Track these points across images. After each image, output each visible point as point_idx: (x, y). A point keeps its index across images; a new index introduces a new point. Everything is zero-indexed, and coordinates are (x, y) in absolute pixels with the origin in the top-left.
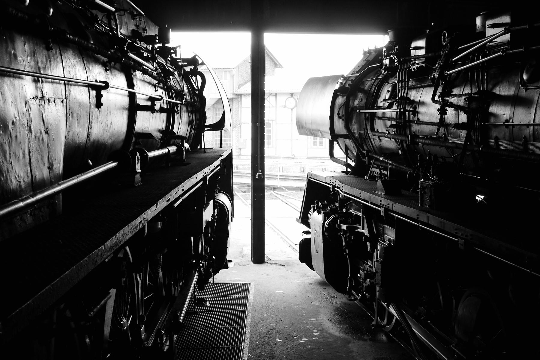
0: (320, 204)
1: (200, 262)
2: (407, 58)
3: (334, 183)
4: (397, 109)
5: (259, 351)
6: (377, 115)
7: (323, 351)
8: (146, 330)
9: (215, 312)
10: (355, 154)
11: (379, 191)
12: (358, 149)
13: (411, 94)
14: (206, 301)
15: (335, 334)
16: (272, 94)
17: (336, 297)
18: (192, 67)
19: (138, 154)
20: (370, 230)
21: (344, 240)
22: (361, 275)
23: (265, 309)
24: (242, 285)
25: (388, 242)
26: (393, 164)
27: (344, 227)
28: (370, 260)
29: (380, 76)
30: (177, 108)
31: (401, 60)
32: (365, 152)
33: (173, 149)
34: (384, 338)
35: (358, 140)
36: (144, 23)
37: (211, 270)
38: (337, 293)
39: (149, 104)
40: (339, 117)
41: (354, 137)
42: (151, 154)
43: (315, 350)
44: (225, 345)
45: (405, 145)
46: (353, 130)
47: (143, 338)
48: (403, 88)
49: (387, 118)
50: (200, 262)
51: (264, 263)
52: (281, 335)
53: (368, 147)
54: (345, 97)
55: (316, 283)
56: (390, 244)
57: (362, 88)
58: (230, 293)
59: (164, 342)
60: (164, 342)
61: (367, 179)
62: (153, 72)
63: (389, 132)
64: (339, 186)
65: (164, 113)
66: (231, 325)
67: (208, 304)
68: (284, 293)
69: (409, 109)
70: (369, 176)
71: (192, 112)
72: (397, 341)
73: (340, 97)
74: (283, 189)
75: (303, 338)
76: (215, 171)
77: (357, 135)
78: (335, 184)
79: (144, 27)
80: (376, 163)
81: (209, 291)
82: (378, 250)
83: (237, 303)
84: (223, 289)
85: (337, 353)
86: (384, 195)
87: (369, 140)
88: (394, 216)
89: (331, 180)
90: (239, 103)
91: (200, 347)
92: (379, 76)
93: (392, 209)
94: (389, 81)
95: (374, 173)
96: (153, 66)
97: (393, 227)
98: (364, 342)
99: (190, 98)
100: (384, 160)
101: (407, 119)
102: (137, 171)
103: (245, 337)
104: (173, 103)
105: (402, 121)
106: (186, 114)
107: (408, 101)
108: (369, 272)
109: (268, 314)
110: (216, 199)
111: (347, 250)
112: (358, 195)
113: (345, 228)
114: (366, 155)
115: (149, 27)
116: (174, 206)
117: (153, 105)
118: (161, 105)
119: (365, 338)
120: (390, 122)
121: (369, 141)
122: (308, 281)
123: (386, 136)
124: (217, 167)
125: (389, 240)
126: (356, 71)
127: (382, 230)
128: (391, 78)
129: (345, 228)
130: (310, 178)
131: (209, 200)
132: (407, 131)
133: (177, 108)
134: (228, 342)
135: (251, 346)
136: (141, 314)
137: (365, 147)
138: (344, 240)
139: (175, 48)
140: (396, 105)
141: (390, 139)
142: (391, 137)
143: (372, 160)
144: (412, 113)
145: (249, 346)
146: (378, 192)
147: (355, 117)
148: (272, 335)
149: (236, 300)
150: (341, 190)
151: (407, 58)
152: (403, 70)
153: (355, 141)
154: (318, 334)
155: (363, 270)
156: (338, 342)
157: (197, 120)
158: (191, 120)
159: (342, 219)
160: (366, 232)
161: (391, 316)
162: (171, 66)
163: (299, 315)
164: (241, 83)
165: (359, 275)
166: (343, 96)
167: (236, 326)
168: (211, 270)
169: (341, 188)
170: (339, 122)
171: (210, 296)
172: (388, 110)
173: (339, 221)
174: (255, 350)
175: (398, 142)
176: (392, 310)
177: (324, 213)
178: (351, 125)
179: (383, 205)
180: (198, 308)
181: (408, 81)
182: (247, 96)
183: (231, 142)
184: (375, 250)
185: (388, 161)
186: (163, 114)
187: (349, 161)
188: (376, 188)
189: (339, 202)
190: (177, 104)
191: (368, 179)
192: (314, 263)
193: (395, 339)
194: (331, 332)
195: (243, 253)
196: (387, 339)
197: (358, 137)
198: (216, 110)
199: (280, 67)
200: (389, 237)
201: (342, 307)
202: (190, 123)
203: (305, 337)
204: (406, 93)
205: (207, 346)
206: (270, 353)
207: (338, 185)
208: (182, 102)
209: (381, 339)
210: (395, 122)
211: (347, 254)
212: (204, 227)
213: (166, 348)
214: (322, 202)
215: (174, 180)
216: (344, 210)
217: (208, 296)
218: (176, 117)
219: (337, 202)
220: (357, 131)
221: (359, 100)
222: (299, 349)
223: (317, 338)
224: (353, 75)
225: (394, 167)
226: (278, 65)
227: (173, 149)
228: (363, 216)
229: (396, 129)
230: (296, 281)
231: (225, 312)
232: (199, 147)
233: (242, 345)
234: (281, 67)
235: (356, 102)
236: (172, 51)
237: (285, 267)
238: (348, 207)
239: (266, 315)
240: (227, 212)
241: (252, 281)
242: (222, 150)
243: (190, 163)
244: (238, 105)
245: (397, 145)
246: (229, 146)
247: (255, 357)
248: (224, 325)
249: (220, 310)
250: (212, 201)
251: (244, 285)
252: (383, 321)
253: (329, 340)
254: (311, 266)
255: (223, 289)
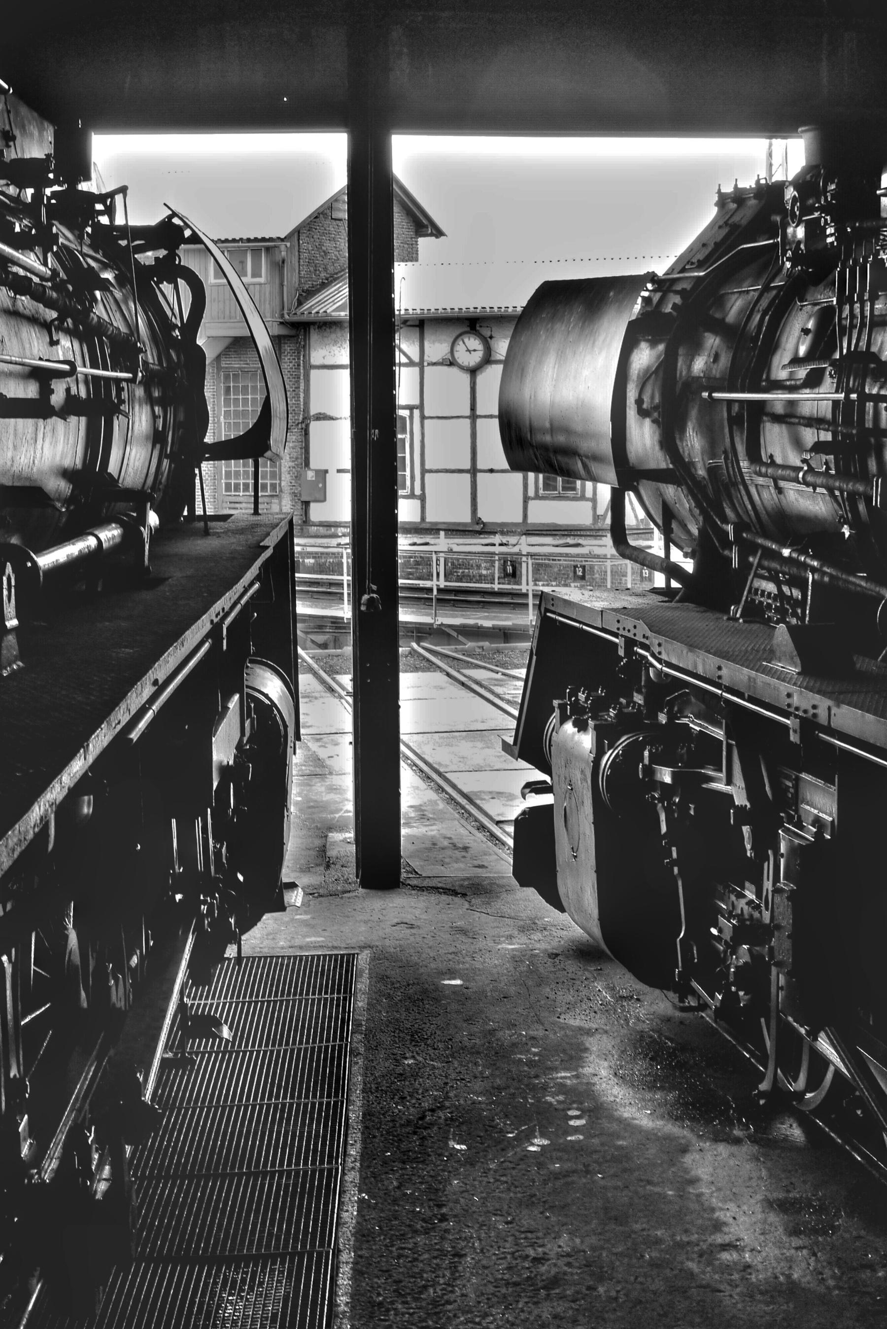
0: (582, 696)
1: (202, 898)
2: (869, 224)
3: (629, 631)
4: (837, 392)
5: (395, 1183)
6: (768, 409)
7: (602, 1178)
8: (32, 1130)
9: (245, 1053)
10: (695, 531)
11: (780, 661)
12: (707, 519)
13: (882, 343)
14: (218, 1024)
15: (636, 1122)
16: (408, 323)
17: (638, 1000)
18: (162, 253)
19: (9, 569)
20: (753, 788)
21: (663, 817)
22: (720, 931)
23: (408, 1042)
24: (330, 961)
25: (815, 830)
26: (825, 569)
27: (666, 776)
28: (752, 883)
29: (777, 280)
30: (119, 395)
31: (849, 230)
32: (730, 528)
33: (110, 534)
34: (795, 1133)
35: (705, 486)
36: (6, 115)
37: (232, 921)
38: (640, 986)
39: (30, 391)
40: (643, 413)
41: (693, 477)
42: (46, 560)
43: (574, 1178)
44: (281, 1164)
45: (862, 507)
46: (689, 454)
47: (26, 1156)
48: (855, 321)
49: (804, 418)
50: (202, 898)
51: (399, 887)
52: (464, 1128)
53: (740, 511)
54: (661, 347)
55: (571, 952)
56: (818, 835)
57: (717, 319)
58: (290, 988)
59: (93, 1168)
60: (93, 1168)
61: (738, 616)
62: (44, 283)
63: (809, 465)
64: (647, 642)
65: (78, 414)
66: (299, 1097)
67: (226, 1033)
68: (467, 988)
69: (875, 391)
70: (744, 606)
71: (163, 402)
72: (839, 1141)
73: (644, 345)
74: (449, 635)
75: (536, 1137)
76: (243, 601)
77: (701, 472)
78: (635, 635)
79: (7, 128)
80: (766, 563)
81: (223, 983)
82: (782, 855)
83: (317, 1023)
84: (268, 976)
85: (648, 1187)
86: (798, 674)
87: (741, 487)
88: (833, 746)
89: (618, 621)
90: (302, 353)
91: (200, 1169)
92: (772, 280)
93: (826, 724)
94: (809, 297)
95: (756, 594)
96: (45, 264)
97: (829, 780)
98: (734, 1149)
99: (156, 359)
100: (795, 555)
101: (869, 424)
102: (7, 623)
103: (346, 1135)
104: (107, 380)
105: (854, 432)
106: (146, 409)
107: (872, 366)
108: (748, 923)
109: (418, 1058)
110: (248, 687)
111: (674, 849)
112: (711, 673)
113: (668, 779)
114: (731, 537)
115: (23, 128)
116: (132, 740)
117: (46, 391)
118: (68, 390)
119: (737, 1132)
120: (813, 433)
121: (743, 492)
122: (543, 946)
123: (801, 480)
124: (251, 584)
125: (817, 822)
126: (695, 260)
127: (792, 790)
128: (813, 288)
129: (668, 779)
130: (547, 610)
131: (227, 698)
132: (869, 463)
133: (119, 395)
134: (291, 1154)
135: (369, 1167)
136: (15, 1076)
137: (729, 512)
138: (663, 817)
139: (111, 195)
140: (831, 376)
141: (815, 489)
142: (819, 480)
143: (754, 554)
144: (885, 405)
145: (361, 1164)
146: (778, 665)
147: (694, 413)
148: (436, 1128)
149: (312, 1012)
150: (653, 655)
151: (868, 224)
152: (856, 262)
153: (695, 488)
154: (582, 1122)
155: (730, 915)
156: (647, 1149)
157: (177, 425)
158: (160, 429)
159: (657, 749)
160: (740, 799)
161: (820, 1062)
162: (94, 254)
163: (520, 1060)
164: (306, 287)
165: (714, 931)
166: (653, 344)
167: (317, 1101)
168: (232, 921)
169: (656, 650)
170: (641, 426)
171: (226, 998)
172: (805, 395)
173: (646, 753)
174: (382, 1181)
175: (840, 499)
176: (825, 1046)
177: (596, 728)
178: (681, 440)
179: (797, 709)
180: (193, 1045)
181: (873, 299)
182: (328, 330)
183: (278, 482)
184: (770, 852)
185: (809, 561)
186: (76, 418)
187: (677, 555)
188: (772, 651)
189: (647, 692)
190: (118, 381)
191: (741, 616)
192: (565, 885)
193: (832, 1135)
194: (626, 1115)
195: (329, 854)
196: (806, 1137)
197: (704, 478)
198: (227, 377)
199: (431, 235)
200: (816, 812)
201: (659, 1032)
202: (157, 437)
203: (543, 1135)
204: (865, 337)
205: (225, 1168)
206: (430, 1187)
207: (644, 636)
208: (135, 375)
209: (787, 1136)
210: (830, 433)
211: (674, 863)
212: (214, 788)
213: (102, 1187)
214: (591, 690)
215: (126, 647)
216: (663, 718)
217: (219, 998)
218: (116, 423)
219: (639, 692)
220: (703, 459)
221: (709, 356)
222: (524, 1175)
223: (581, 1137)
224: (687, 275)
225: (826, 579)
226: (426, 227)
227: (110, 534)
228: (730, 741)
229: (832, 457)
230: (504, 945)
231: (279, 1052)
232: (185, 513)
233: (337, 1163)
234: (438, 233)
235: (699, 365)
236: (99, 207)
237: (468, 898)
238: (676, 709)
239: (411, 1061)
240: (282, 728)
241: (362, 948)
242: (261, 525)
243: (166, 579)
244: (299, 359)
245: (835, 505)
246: (269, 493)
247: (382, 1204)
248: (277, 1098)
249: (260, 1046)
250: (237, 697)
251: (336, 960)
252: (795, 1080)
253: (620, 1143)
254: (555, 901)
255: (268, 976)
